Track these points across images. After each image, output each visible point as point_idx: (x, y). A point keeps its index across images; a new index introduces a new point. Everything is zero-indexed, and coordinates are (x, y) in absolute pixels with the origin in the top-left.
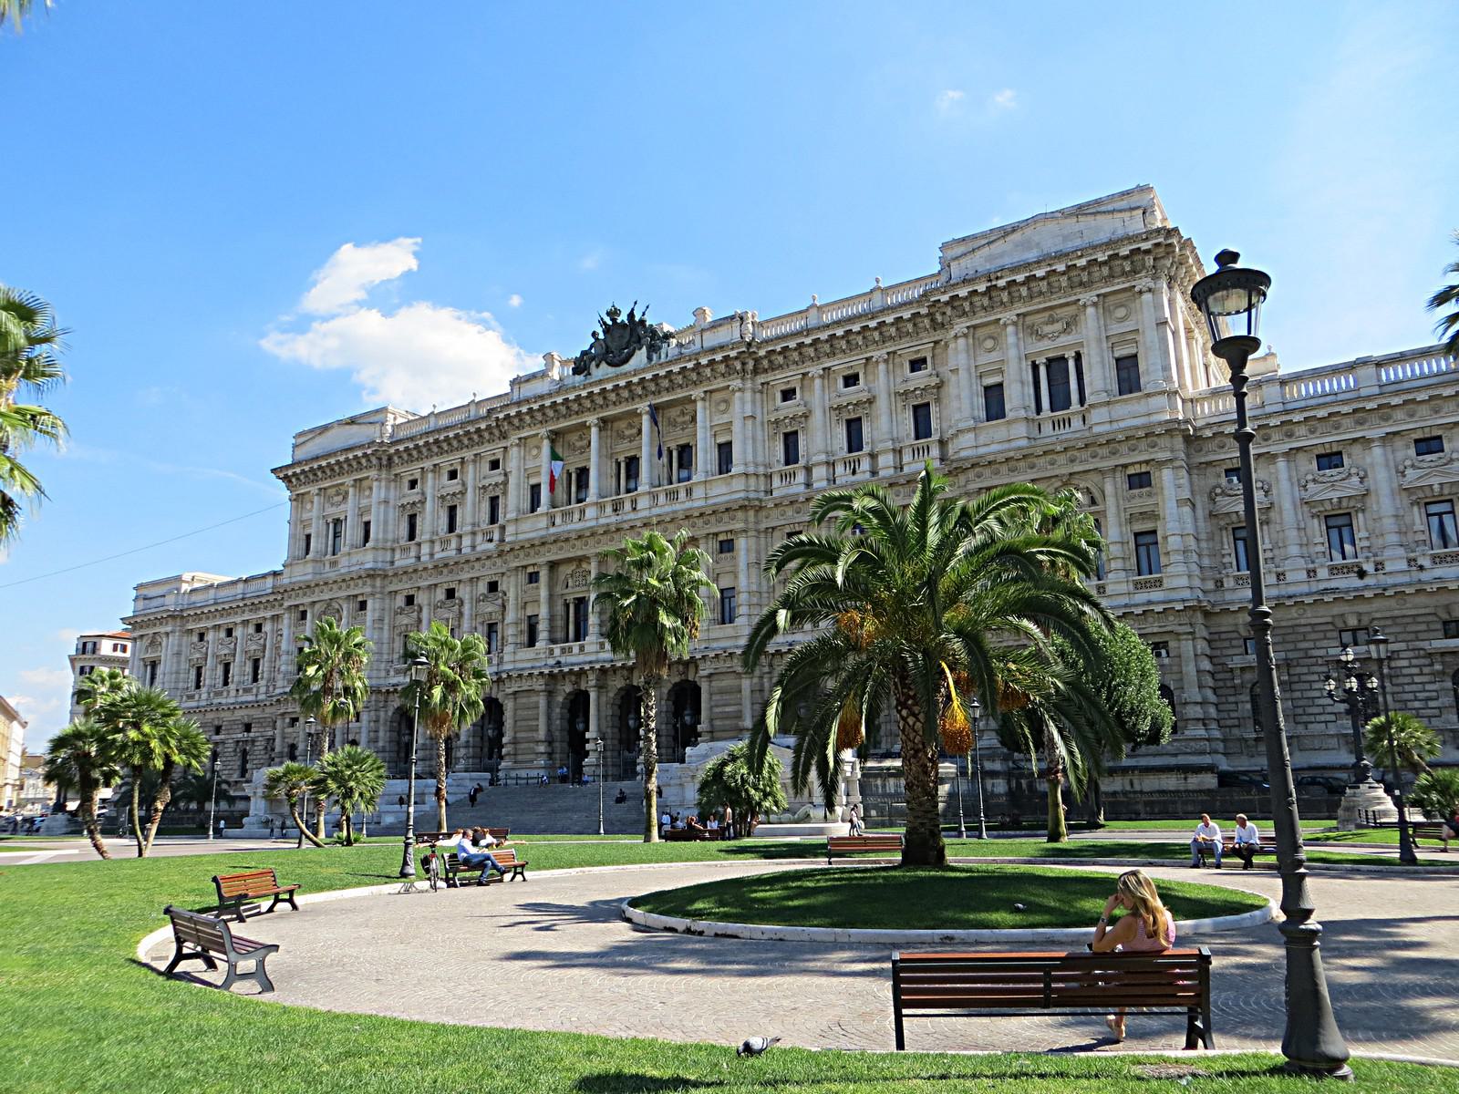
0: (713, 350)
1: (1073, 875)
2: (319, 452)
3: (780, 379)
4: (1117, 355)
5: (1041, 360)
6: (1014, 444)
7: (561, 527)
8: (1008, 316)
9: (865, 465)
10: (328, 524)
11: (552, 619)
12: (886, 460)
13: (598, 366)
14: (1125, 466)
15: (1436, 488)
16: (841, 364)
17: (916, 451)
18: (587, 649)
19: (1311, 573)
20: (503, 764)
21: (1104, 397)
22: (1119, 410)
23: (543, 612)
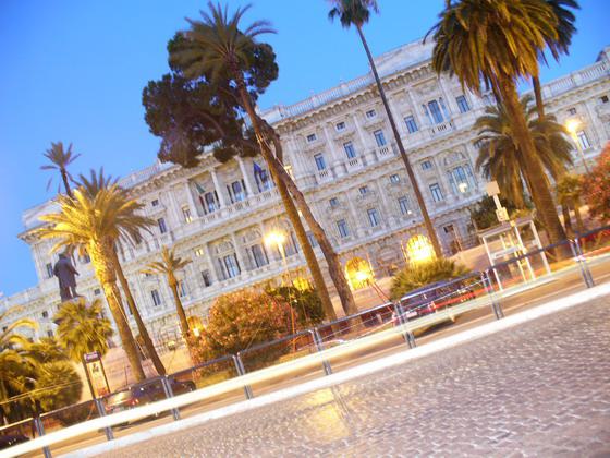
1: (569, 309)
3: (306, 132)
7: (209, 225)
8: (407, 87)
11: (216, 269)
12: (369, 158)
16: (334, 119)
17: (322, 175)
19: (367, 233)
21: (457, 115)
22: (464, 118)
23: (211, 267)
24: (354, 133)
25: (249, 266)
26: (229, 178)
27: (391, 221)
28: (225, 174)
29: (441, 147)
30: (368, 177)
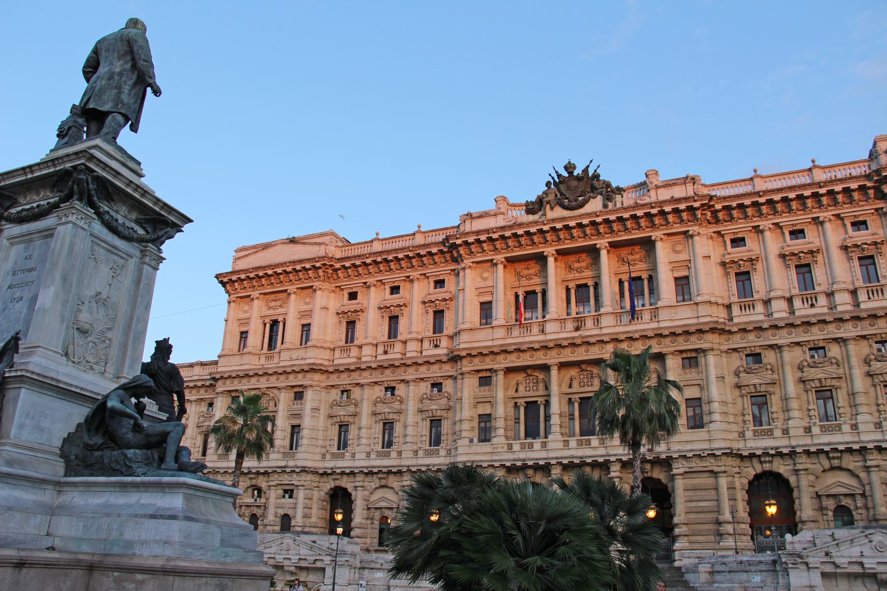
0: (478, 233)
2: (263, 264)
3: (730, 229)
4: (676, 275)
5: (572, 285)
6: (702, 320)
7: (517, 338)
8: (764, 224)
9: (822, 300)
10: (265, 324)
13: (552, 209)
18: (550, 446)
19: (808, 430)
20: (677, 545)
24: (451, 299)
25: (511, 434)
26: (524, 282)
27: (865, 419)
28: (570, 269)
30: (833, 331)
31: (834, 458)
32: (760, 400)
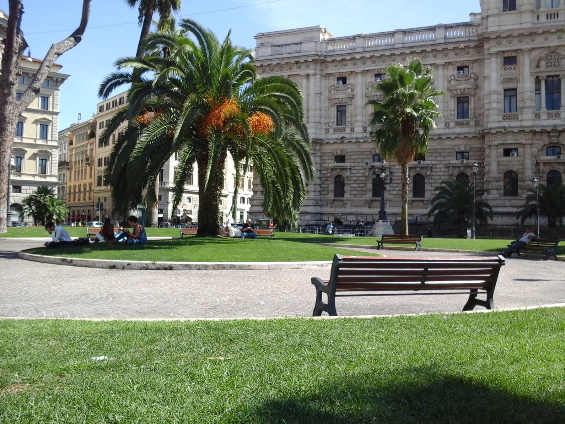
6: (523, 26)
14: (504, 52)
15: (340, 99)
21: (496, 11)
29: (539, 42)
31: (552, 136)
32: (341, 110)
